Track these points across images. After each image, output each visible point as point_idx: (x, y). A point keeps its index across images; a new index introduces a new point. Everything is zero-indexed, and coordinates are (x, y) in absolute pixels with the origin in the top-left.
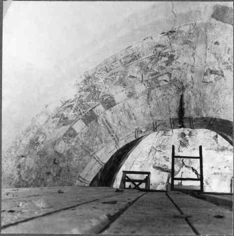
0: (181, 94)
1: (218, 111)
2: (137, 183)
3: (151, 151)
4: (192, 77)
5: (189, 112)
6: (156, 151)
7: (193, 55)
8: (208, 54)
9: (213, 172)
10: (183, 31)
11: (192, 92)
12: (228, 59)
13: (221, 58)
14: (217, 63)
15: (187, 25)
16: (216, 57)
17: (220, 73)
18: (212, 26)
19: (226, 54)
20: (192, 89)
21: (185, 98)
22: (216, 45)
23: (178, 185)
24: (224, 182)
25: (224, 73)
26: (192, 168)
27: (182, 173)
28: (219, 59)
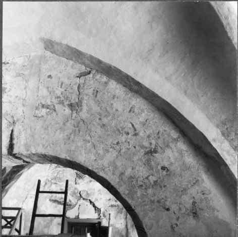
0: (11, 129)
1: (47, 147)
2: (9, 220)
3: (46, 183)
4: (23, 110)
5: (19, 147)
6: (52, 183)
7: (25, 88)
8: (40, 87)
9: (110, 204)
10: (17, 63)
11: (23, 126)
12: (60, 93)
13: (54, 92)
14: (49, 97)
15: (21, 56)
16: (48, 91)
17: (52, 107)
18: (46, 59)
19: (60, 88)
20: (23, 124)
21: (15, 133)
22: (50, 79)
23: (75, 218)
24: (120, 215)
25: (56, 108)
26: (90, 200)
27: (80, 206)
28: (52, 93)
